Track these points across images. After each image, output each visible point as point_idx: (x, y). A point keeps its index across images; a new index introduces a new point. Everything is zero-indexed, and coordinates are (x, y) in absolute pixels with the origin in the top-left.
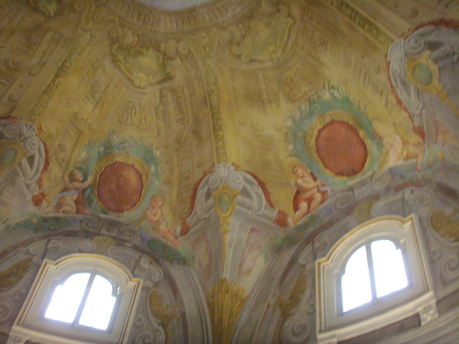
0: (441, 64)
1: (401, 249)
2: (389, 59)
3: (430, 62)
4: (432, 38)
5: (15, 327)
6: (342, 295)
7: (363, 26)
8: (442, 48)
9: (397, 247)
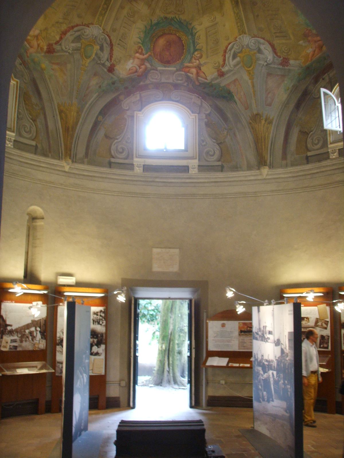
2: (91, 26)
4: (105, 45)
8: (101, 53)
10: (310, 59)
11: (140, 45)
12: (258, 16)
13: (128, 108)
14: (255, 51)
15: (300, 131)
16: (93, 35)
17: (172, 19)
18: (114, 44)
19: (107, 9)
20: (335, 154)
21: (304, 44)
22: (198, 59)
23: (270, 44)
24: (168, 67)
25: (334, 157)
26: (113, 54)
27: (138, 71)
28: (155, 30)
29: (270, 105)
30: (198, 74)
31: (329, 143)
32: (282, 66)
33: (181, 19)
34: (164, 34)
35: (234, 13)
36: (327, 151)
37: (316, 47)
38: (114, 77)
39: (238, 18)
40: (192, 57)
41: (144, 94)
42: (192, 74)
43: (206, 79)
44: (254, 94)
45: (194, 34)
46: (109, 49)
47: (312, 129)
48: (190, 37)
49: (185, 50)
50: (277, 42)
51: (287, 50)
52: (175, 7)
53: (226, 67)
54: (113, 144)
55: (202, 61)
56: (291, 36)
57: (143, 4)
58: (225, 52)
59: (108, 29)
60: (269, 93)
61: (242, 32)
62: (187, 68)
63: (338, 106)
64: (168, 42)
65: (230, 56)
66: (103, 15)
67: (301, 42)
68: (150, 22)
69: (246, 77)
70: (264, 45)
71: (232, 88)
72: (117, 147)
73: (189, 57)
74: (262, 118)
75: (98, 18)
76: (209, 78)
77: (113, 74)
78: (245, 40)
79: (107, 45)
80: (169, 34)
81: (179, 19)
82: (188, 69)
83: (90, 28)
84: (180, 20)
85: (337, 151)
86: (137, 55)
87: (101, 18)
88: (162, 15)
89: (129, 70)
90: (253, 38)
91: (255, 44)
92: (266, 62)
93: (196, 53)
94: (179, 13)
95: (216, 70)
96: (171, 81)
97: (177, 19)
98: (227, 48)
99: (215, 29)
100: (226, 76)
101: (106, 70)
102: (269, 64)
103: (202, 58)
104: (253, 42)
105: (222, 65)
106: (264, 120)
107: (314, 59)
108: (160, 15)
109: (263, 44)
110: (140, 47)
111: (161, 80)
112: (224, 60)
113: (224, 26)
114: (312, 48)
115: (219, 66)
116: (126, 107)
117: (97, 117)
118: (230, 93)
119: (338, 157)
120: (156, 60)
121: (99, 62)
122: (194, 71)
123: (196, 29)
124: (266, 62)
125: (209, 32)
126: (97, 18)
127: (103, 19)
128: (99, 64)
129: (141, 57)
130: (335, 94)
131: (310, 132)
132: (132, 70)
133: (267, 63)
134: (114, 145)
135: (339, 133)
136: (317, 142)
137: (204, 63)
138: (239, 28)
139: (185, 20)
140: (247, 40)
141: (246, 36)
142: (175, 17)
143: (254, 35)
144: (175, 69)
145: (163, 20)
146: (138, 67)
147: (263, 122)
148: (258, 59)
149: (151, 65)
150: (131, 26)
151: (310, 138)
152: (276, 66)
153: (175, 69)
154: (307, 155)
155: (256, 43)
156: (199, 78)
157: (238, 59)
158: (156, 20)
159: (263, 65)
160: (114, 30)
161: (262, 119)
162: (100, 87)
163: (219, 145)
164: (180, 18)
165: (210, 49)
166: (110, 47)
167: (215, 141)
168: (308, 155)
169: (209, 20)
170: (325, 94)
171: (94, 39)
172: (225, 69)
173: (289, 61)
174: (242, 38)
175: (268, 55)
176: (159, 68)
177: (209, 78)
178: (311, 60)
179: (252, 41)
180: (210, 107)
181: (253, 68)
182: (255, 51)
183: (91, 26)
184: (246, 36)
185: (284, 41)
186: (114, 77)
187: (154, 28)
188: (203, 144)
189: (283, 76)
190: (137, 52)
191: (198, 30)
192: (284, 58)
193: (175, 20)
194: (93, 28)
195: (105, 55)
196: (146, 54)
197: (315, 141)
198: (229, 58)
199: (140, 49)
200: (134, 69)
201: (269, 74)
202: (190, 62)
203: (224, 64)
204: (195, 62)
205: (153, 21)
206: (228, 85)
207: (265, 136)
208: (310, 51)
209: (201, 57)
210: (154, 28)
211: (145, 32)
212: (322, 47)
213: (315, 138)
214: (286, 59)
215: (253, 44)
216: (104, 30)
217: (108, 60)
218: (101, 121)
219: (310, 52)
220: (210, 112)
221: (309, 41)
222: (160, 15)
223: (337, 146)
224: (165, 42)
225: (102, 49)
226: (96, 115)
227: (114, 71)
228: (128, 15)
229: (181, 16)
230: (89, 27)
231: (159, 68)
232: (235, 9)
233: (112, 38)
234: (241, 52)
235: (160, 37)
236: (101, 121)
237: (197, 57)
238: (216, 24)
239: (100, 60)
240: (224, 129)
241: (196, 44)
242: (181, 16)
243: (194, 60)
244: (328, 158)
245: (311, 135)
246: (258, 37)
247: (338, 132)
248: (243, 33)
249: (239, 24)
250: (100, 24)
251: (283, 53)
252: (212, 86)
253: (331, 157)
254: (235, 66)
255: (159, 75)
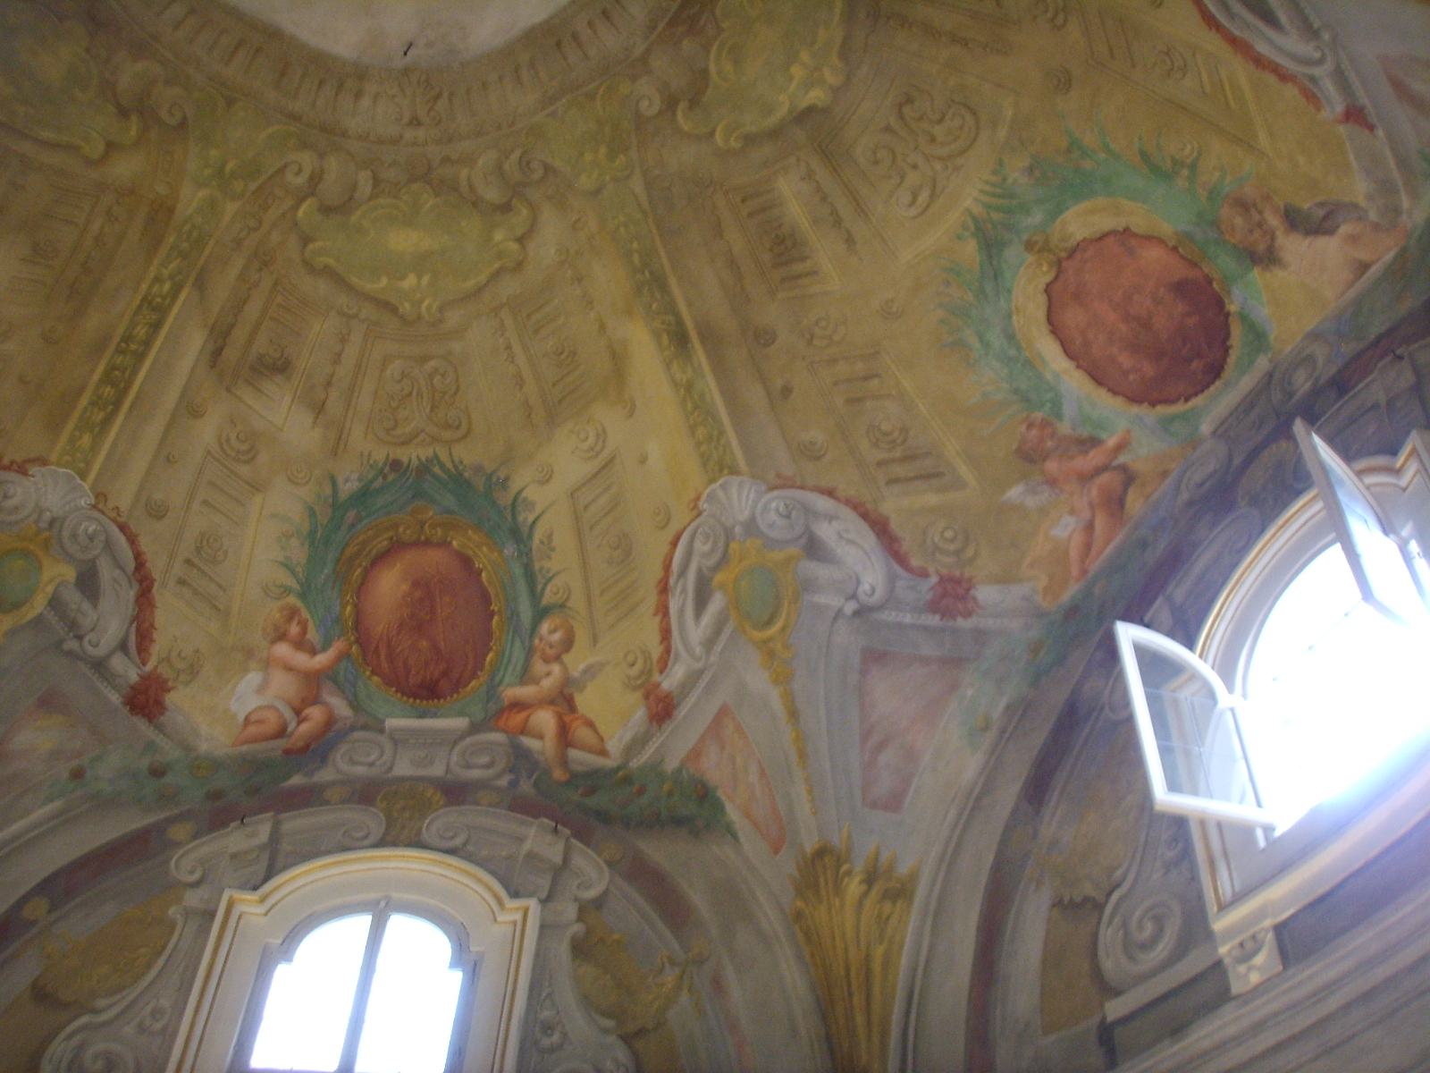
0: (52, 618)
1: (463, 971)
2: (33, 470)
3: (50, 589)
4: (106, 571)
5: (1219, 925)
6: (375, 970)
7: (107, 379)
8: (86, 606)
9: (457, 961)
10: (1075, 571)
11: (292, 600)
12: (787, 391)
13: (196, 876)
14: (793, 550)
15: (1058, 904)
16: (40, 511)
17: (424, 469)
18: (156, 575)
19: (117, 404)
20: (1259, 959)
21: (1031, 502)
22: (558, 658)
23: (865, 516)
24: (435, 715)
25: (1255, 978)
26: (152, 626)
27: (289, 729)
28: (353, 525)
29: (893, 803)
30: (565, 737)
31: (1215, 909)
32: (937, 617)
33: (461, 462)
34: (396, 547)
35: (675, 384)
36: (1208, 962)
37: (1091, 505)
38: (159, 739)
39: (696, 407)
40: (530, 652)
41: (297, 823)
42: (541, 737)
43: (603, 753)
44: (802, 755)
45: (525, 530)
46: (132, 593)
47: (1118, 873)
48: (510, 549)
49: (496, 618)
50: (892, 505)
51: (952, 540)
52: (428, 410)
53: (677, 667)
54: (63, 1035)
55: (577, 662)
56: (964, 471)
57: (287, 399)
58: (664, 589)
59: (124, 496)
60: (882, 745)
61: (719, 467)
62: (518, 712)
63: (1232, 710)
64: (416, 584)
65: (685, 600)
66: (97, 430)
67: (1015, 493)
68: (328, 491)
69: (757, 679)
70: (834, 523)
71: (713, 769)
72: (81, 1047)
73: (518, 653)
74: (845, 867)
75: (72, 440)
76: (615, 746)
77: (160, 729)
78: (735, 496)
79: (118, 571)
80: (417, 544)
81: (453, 462)
82: (522, 715)
83: (33, 476)
84: (455, 466)
85: (1270, 936)
86: (283, 650)
87: (86, 440)
88: (380, 455)
89: (247, 721)
90: (776, 493)
91: (788, 517)
92: (854, 596)
93: (545, 627)
94: (447, 435)
95: (639, 695)
96: (437, 770)
97: (442, 466)
98: (667, 567)
99: (609, 487)
100: (683, 713)
101: (115, 698)
102: (871, 609)
103: (574, 650)
104: (777, 510)
105: (658, 662)
106: (857, 879)
107: (1095, 566)
108: (370, 455)
109: (831, 518)
110: (292, 614)
111: (391, 769)
112: (666, 634)
113: (643, 460)
114: (1072, 512)
115: (650, 671)
116: (192, 872)
117: (25, 899)
118: (704, 794)
119: (1278, 975)
120: (375, 678)
121: (72, 645)
122: (545, 719)
123: (530, 505)
124: (854, 596)
125: (586, 507)
126: (64, 437)
127: (95, 448)
128: (70, 653)
129: (302, 660)
130: (1211, 657)
131: (1109, 894)
132: (259, 722)
133: (858, 602)
134: (70, 1037)
135: (1262, 843)
136: (1149, 927)
137: (585, 672)
138: (704, 448)
139: (478, 469)
140: (742, 499)
141: (741, 485)
142: (436, 456)
143: (779, 476)
144: (460, 723)
145: (385, 477)
146: (288, 714)
147: (854, 887)
148: (808, 585)
149: (355, 705)
150: (243, 505)
151: (1110, 923)
152: (908, 619)
153: (460, 723)
154: (1104, 1018)
155: (794, 514)
156: (573, 754)
157: (716, 603)
158: (355, 476)
159: (839, 613)
160: (157, 512)
161: (849, 873)
162: (78, 774)
163: (630, 1047)
164: (456, 460)
165: (602, 593)
166: (136, 586)
167: (609, 1023)
168: (1110, 1019)
169: (577, 448)
170: (1153, 663)
171: (43, 525)
172: (671, 681)
173: (972, 592)
174: (720, 494)
175: (860, 563)
176: (393, 723)
177: (615, 746)
178: (1084, 572)
179: (774, 505)
180: (606, 868)
181: (783, 629)
182: (793, 550)
183: (33, 470)
184: (741, 485)
185: (932, 499)
186: (159, 739)
187: (351, 514)
188: (546, 1042)
189: (954, 662)
190: (281, 637)
191: (538, 510)
192: (943, 580)
193: (436, 470)
194: (43, 476)
195: (108, 622)
196: (324, 649)
197: (1141, 927)
198: (682, 611)
199: (295, 622)
200: (272, 718)
201: (875, 657)
202: (525, 677)
203: (668, 651)
204: (548, 674)
205: (340, 480)
206: (696, 754)
207: (868, 958)
208: (1065, 528)
209: (568, 643)
210: (351, 514)
211: (312, 533)
212: (1121, 503)
213: (1138, 913)
214: (958, 582)
215: (781, 515)
216: (101, 496)
217: (123, 647)
218: (34, 923)
219: (1070, 537)
220: (606, 893)
221: (1052, 482)
222: (370, 455)
223: (1261, 914)
224: (405, 587)
225: (88, 583)
226: (23, 890)
227: (162, 714)
228: (222, 449)
229: (460, 452)
230: (25, 473)
231: (393, 723)
232: (675, 366)
233: (145, 544)
234: (724, 560)
235: (381, 559)
236: (34, 923)
237: (551, 647)
238: (610, 462)
239: (80, 638)
240: (667, 965)
241: (540, 581)
242: (460, 452)
243: (539, 667)
244: (1223, 996)
245: (1118, 905)
246: (802, 488)
247: (1259, 834)
248: (726, 471)
249: (701, 432)
250: (82, 465)
251: (938, 555)
252: (627, 780)
253: (1236, 988)
254: (709, 643)
255: (389, 747)
